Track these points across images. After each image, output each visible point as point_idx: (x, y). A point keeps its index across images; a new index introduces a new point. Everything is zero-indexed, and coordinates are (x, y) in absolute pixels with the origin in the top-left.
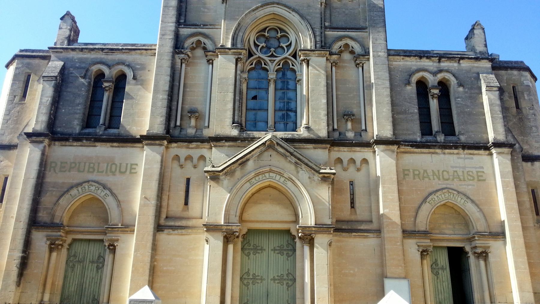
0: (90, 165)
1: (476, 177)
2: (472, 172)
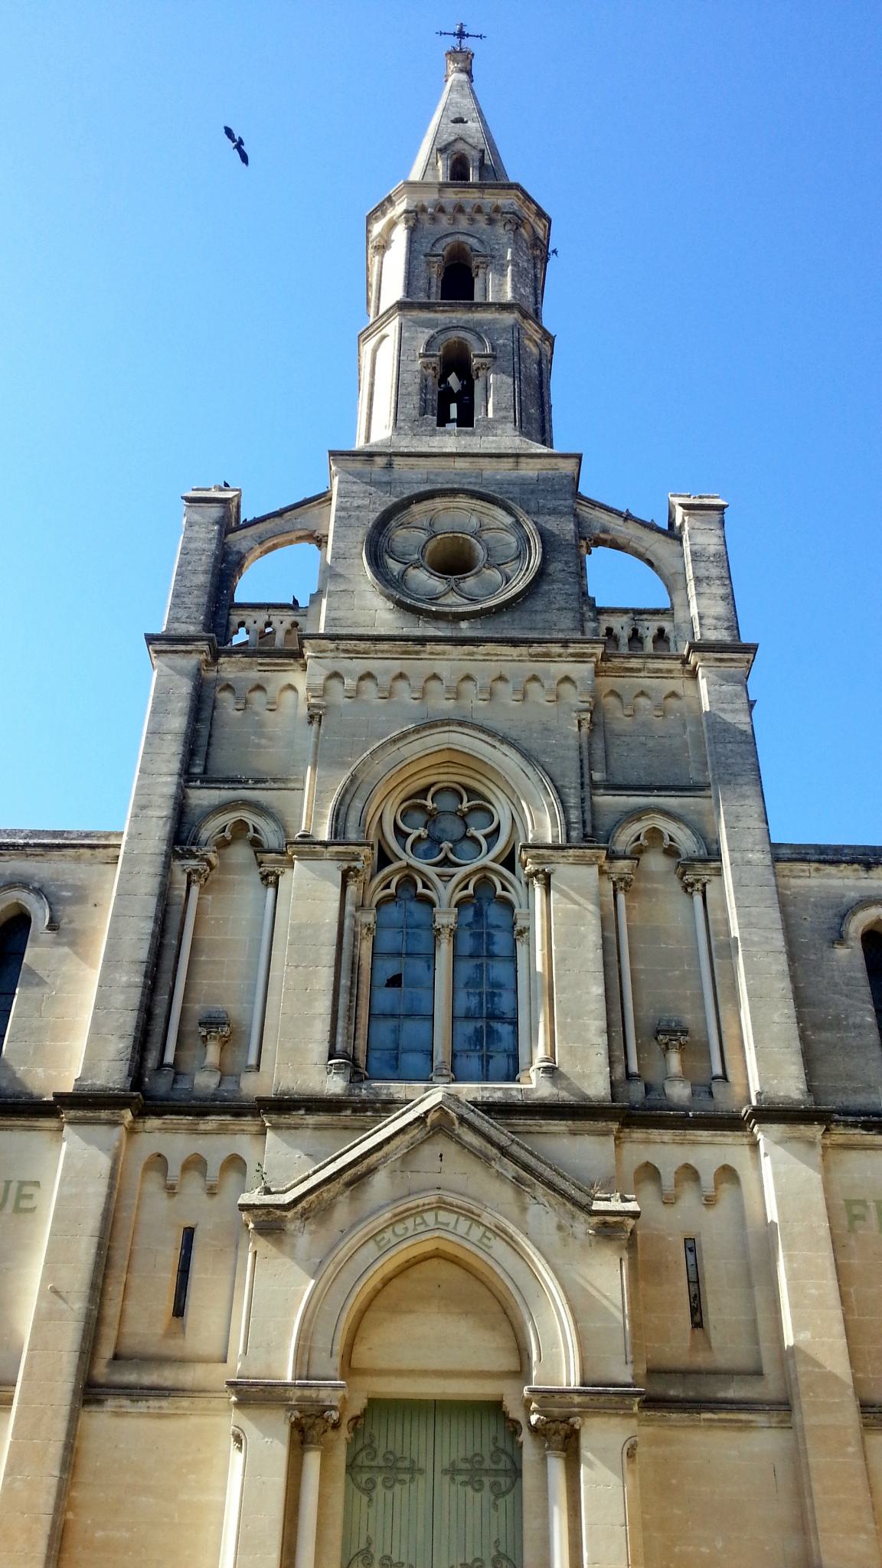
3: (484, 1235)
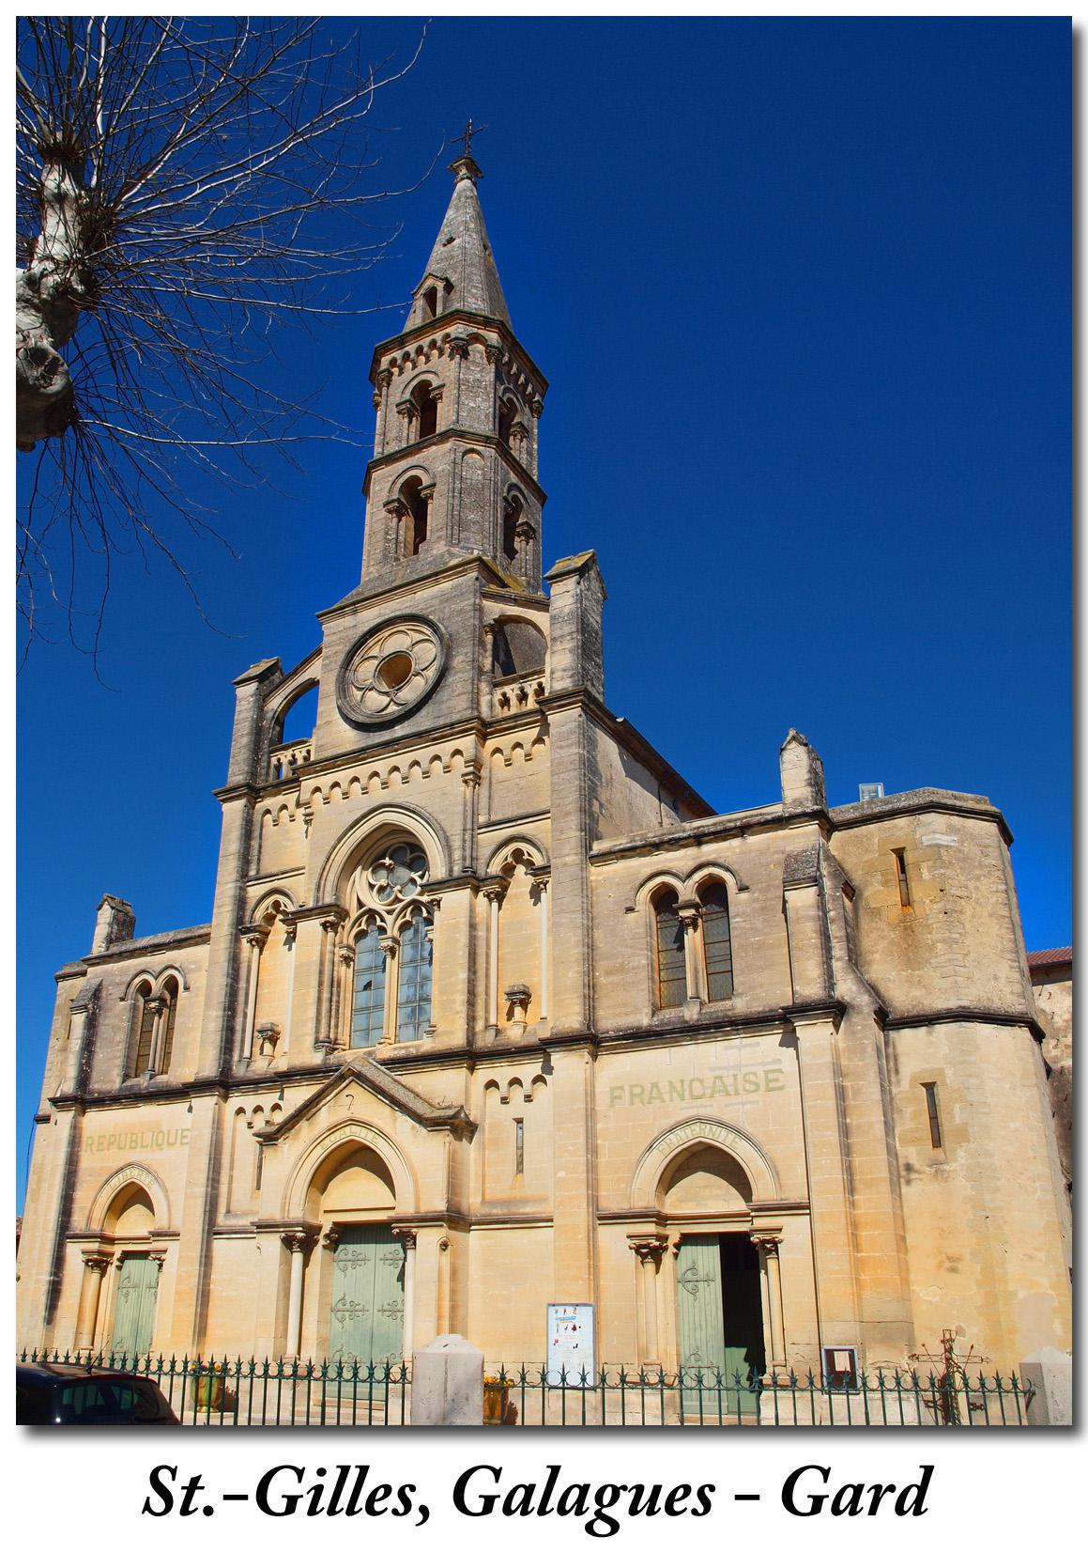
1: (762, 1083)
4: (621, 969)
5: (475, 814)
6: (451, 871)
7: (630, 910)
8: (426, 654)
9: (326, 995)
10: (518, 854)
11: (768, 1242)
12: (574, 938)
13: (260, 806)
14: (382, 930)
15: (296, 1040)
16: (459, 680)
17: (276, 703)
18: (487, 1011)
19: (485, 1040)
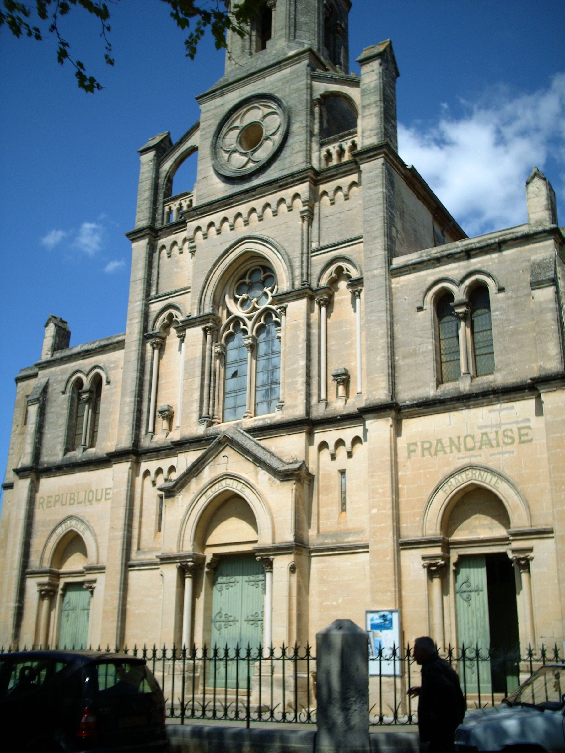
0: (71, 496)
1: (517, 438)
2: (511, 430)
3: (242, 487)
4: (414, 354)
5: (309, 242)
6: (293, 284)
7: (420, 309)
8: (273, 123)
9: (206, 382)
10: (340, 270)
11: (523, 559)
12: (382, 330)
13: (161, 242)
14: (245, 332)
15: (186, 417)
16: (298, 140)
17: (167, 166)
18: (319, 390)
19: (319, 412)
